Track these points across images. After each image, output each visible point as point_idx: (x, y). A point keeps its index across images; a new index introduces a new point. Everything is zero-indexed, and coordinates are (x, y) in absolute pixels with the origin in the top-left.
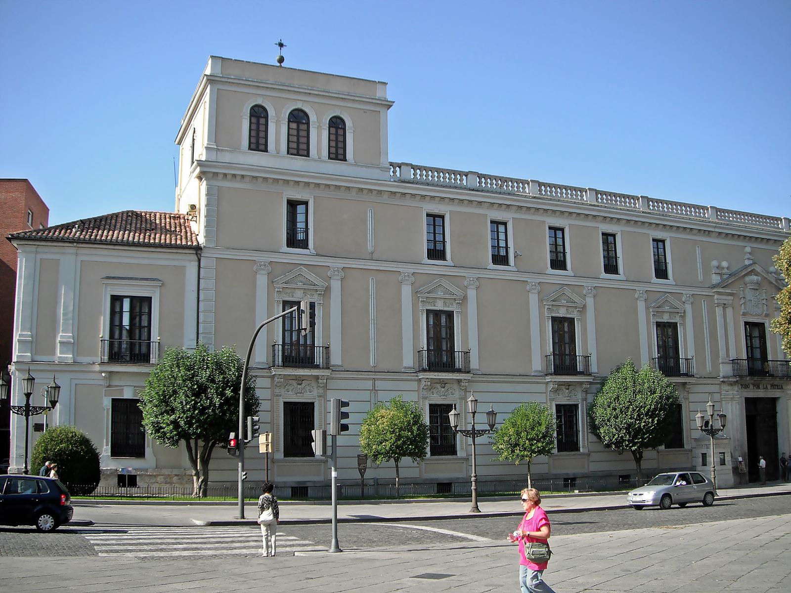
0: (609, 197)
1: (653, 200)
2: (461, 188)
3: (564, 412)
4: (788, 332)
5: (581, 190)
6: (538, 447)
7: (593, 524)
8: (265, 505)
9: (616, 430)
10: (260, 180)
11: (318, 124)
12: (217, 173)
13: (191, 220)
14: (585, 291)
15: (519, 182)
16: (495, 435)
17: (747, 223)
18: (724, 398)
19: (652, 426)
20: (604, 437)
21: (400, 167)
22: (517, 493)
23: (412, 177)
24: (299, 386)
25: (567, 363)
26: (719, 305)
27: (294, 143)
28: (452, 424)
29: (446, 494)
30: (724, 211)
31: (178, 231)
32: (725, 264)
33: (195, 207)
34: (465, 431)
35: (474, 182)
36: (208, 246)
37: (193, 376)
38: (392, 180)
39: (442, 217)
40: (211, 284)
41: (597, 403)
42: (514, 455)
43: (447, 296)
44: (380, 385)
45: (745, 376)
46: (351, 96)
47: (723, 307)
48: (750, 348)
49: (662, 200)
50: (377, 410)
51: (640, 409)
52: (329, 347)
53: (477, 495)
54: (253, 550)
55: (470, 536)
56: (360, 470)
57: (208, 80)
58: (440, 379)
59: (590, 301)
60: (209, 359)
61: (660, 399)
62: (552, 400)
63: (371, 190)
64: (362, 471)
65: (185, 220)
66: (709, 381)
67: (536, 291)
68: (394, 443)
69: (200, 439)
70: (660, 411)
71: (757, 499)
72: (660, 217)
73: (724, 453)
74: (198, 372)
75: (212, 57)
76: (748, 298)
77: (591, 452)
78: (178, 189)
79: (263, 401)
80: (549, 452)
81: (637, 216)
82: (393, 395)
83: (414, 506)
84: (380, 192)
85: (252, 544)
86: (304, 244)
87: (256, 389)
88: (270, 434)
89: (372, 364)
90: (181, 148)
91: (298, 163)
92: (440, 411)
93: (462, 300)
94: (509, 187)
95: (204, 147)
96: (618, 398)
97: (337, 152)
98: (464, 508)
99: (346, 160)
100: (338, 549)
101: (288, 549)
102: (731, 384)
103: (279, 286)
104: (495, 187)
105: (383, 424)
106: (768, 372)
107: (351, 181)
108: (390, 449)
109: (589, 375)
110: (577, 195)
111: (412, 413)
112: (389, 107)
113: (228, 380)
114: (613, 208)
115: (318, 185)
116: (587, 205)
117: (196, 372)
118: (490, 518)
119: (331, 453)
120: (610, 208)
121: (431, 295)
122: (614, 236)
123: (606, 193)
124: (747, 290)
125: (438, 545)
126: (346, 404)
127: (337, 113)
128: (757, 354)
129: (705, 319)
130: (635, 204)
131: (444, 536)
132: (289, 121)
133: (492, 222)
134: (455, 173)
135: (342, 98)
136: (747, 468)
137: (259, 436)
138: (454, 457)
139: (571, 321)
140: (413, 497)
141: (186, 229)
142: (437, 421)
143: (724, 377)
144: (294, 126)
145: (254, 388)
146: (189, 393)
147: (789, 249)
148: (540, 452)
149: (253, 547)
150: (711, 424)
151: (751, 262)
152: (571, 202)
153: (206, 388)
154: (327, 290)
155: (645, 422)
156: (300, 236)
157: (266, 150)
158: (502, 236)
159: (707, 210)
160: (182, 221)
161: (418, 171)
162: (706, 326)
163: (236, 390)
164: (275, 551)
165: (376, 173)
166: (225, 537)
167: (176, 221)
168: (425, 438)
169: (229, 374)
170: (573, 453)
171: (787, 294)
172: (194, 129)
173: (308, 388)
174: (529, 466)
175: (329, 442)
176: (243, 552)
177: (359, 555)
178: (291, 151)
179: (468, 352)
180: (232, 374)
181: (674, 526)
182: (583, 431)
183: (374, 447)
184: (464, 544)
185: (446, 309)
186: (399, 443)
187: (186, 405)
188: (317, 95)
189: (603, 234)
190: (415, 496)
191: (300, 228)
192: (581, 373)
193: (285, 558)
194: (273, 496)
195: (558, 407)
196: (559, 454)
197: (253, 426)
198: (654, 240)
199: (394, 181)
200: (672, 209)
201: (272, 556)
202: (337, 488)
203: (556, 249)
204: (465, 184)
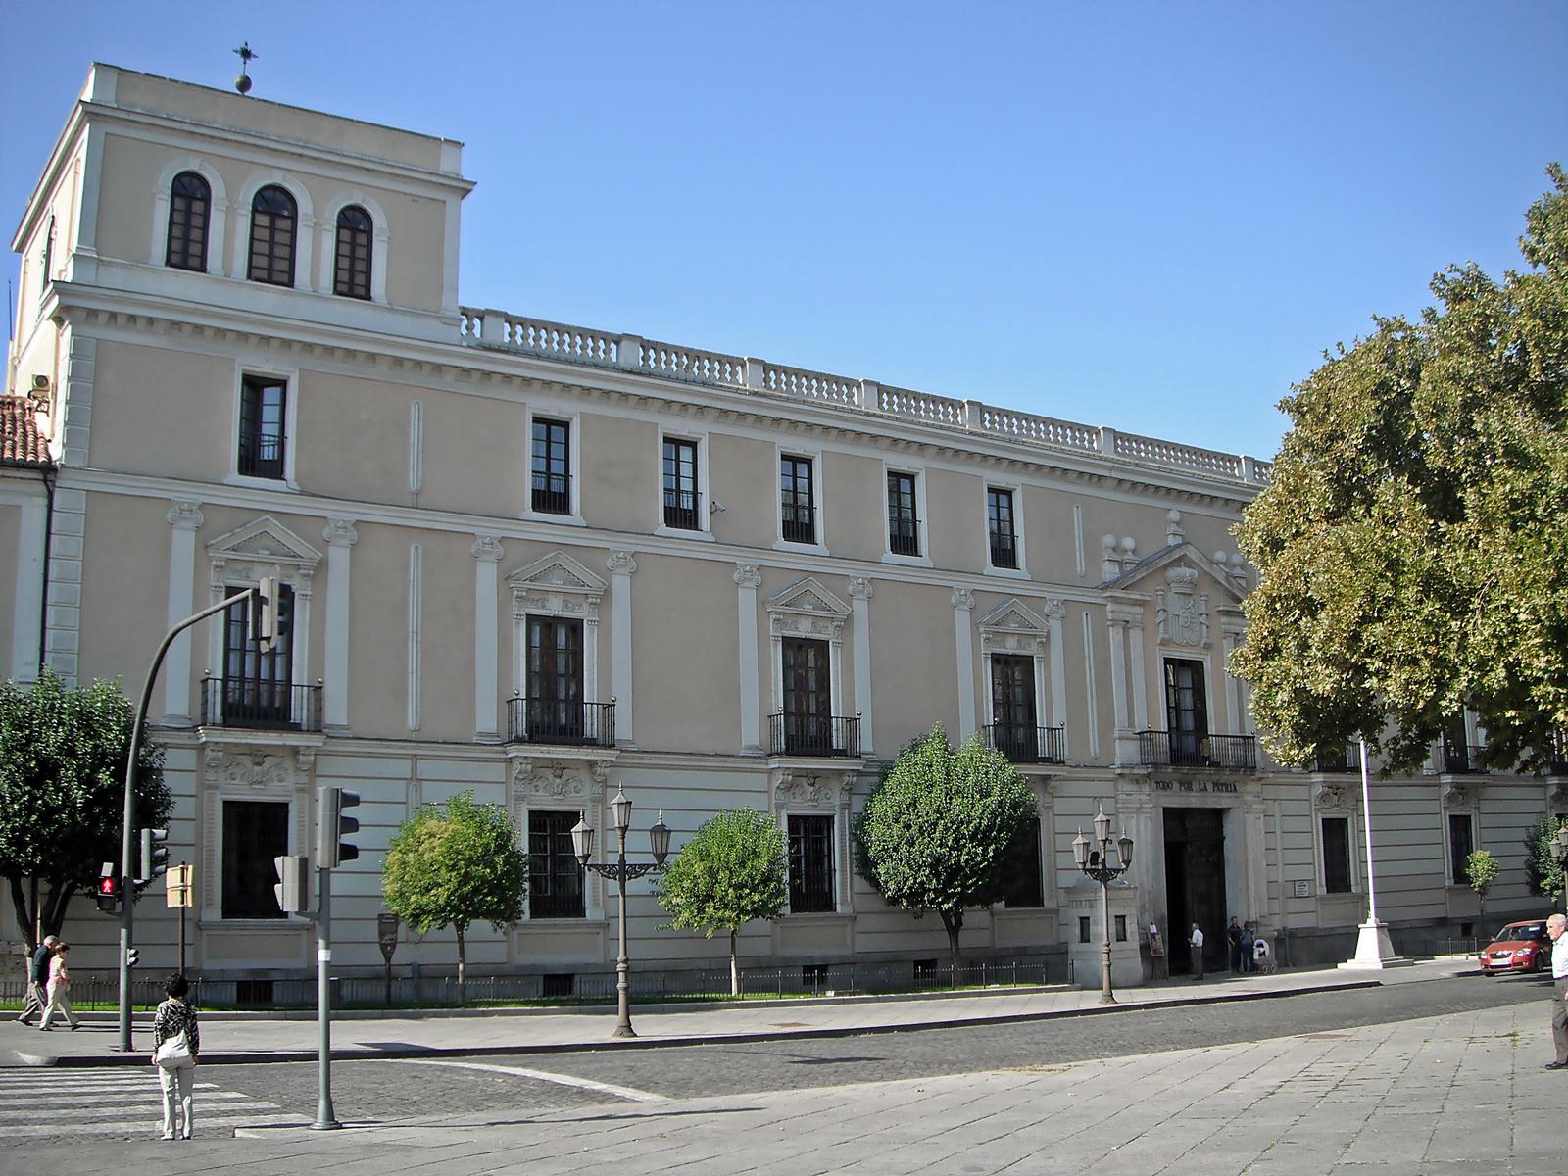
0: (904, 400)
1: (991, 410)
2: (606, 368)
3: (805, 831)
4: (1262, 676)
5: (850, 383)
6: (753, 902)
7: (875, 1064)
8: (172, 1023)
9: (911, 868)
10: (187, 330)
11: (316, 220)
12: (96, 310)
13: (37, 410)
14: (850, 588)
15: (724, 361)
16: (664, 877)
17: (1173, 464)
18: (1122, 808)
19: (983, 861)
20: (886, 882)
21: (481, 319)
22: (710, 995)
23: (507, 339)
24: (257, 768)
25: (813, 730)
26: (1115, 623)
27: (263, 244)
28: (579, 851)
29: (562, 998)
30: (1130, 438)
31: (7, 430)
32: (1128, 543)
33: (47, 381)
34: (604, 867)
35: (634, 356)
36: (68, 465)
37: (30, 739)
38: (465, 344)
39: (566, 425)
40: (75, 545)
41: (871, 814)
42: (703, 918)
43: (570, 588)
44: (426, 768)
45: (1165, 765)
46: (387, 165)
47: (1124, 628)
48: (1175, 710)
49: (1008, 411)
50: (421, 823)
51: (959, 828)
52: (321, 687)
53: (630, 1001)
54: (143, 1123)
55: (620, 1091)
56: (383, 947)
57: (86, 113)
58: (551, 759)
59: (860, 608)
60: (65, 705)
61: (999, 807)
62: (780, 806)
63: (419, 364)
64: (387, 950)
65: (24, 409)
66: (1092, 774)
67: (752, 584)
68: (456, 890)
69: (42, 877)
70: (999, 832)
71: (1193, 1008)
72: (1004, 444)
73: (1124, 917)
74: (40, 733)
75: (97, 65)
76: (1172, 611)
77: (858, 913)
78: (12, 347)
79: (177, 798)
80: (774, 911)
81: (959, 440)
82: (449, 791)
83: (496, 1024)
84: (438, 368)
85: (142, 1109)
86: (275, 470)
87: (163, 772)
88: (191, 867)
89: (411, 723)
90: (24, 258)
91: (268, 299)
92: (551, 827)
93: (601, 597)
94: (703, 370)
95: (71, 254)
96: (914, 804)
97: (353, 281)
98: (602, 1028)
99: (369, 298)
100: (331, 1122)
101: (222, 1121)
102: (1137, 780)
103: (220, 555)
104: (675, 369)
105: (434, 851)
106: (1208, 758)
107: (378, 342)
108: (447, 904)
109: (857, 756)
110: (840, 393)
111: (494, 827)
112: (463, 192)
113: (104, 750)
114: (912, 423)
115: (309, 347)
116: (860, 413)
117: (37, 731)
118: (656, 1049)
119: (318, 908)
120: (905, 421)
121: (538, 585)
122: (911, 478)
123: (898, 392)
124: (1171, 596)
125: (553, 1111)
126: (353, 800)
127: (356, 199)
128: (1188, 722)
129: (1088, 649)
130: (955, 416)
131: (563, 1089)
132: (255, 210)
133: (667, 440)
134: (595, 335)
135: (368, 169)
136: (1167, 949)
137: (166, 872)
138: (579, 920)
139: (822, 647)
140: (493, 1004)
141: (25, 429)
142: (546, 846)
143: (1123, 767)
144: (263, 220)
145: (159, 771)
146: (19, 778)
147: (1266, 512)
148: (756, 912)
149: (143, 1117)
150: (1103, 857)
151: (1179, 540)
152: (828, 407)
153: (57, 766)
154: (321, 567)
155: (968, 853)
156: (268, 453)
157: (202, 269)
158: (686, 470)
159: (1096, 434)
160: (18, 411)
161: (519, 329)
162: (1089, 665)
163: (118, 774)
164: (191, 1126)
165: (432, 329)
166: (84, 1094)
167: (6, 412)
168: (519, 879)
169: (106, 739)
170: (821, 915)
171: (1264, 598)
172: (53, 216)
173: (275, 774)
174: (733, 938)
175: (315, 881)
176: (120, 1128)
177: (381, 1135)
178: (256, 273)
179: (611, 706)
180: (111, 739)
181: (1046, 1067)
182: (843, 871)
183: (413, 898)
184: (608, 1108)
185: (568, 614)
186: (466, 889)
187: (12, 802)
188: (315, 159)
189: (890, 474)
190: (497, 1002)
191: (269, 436)
192: (841, 753)
193: (213, 1145)
194: (188, 1005)
195: (793, 820)
196: (1331, 895)
197: (153, 847)
198: (991, 490)
199: (469, 347)
200: (1029, 430)
201: (184, 1138)
202: (331, 985)
203: (795, 499)
204: (614, 360)
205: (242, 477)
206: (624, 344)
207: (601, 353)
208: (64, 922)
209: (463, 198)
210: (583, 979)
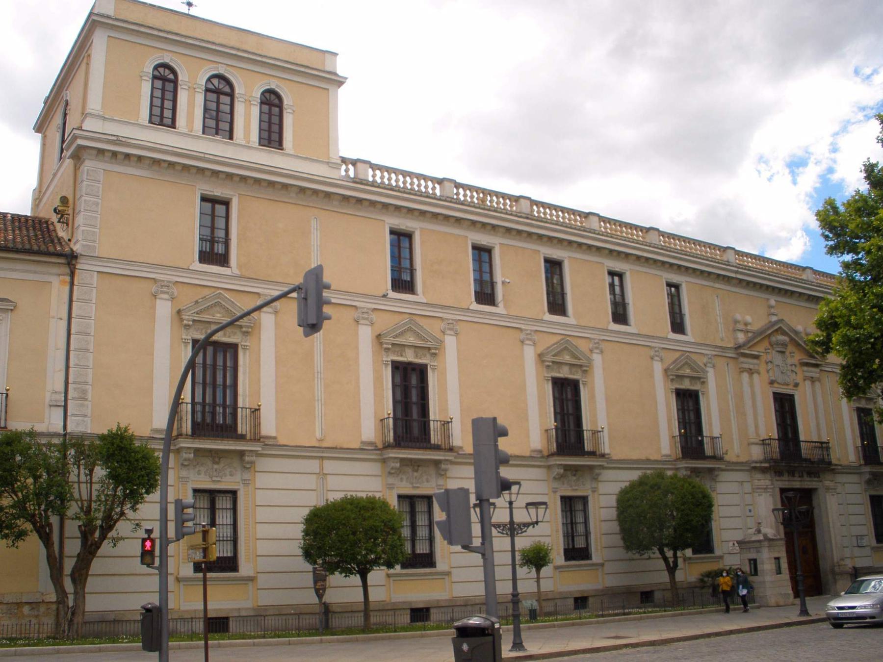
56: (317, 591)
156: (220, 248)
158: (220, 223)
205: (201, 265)
206: (359, 165)
207: (508, 207)
208: (89, 578)
209: (339, 87)
210: (455, 610)
